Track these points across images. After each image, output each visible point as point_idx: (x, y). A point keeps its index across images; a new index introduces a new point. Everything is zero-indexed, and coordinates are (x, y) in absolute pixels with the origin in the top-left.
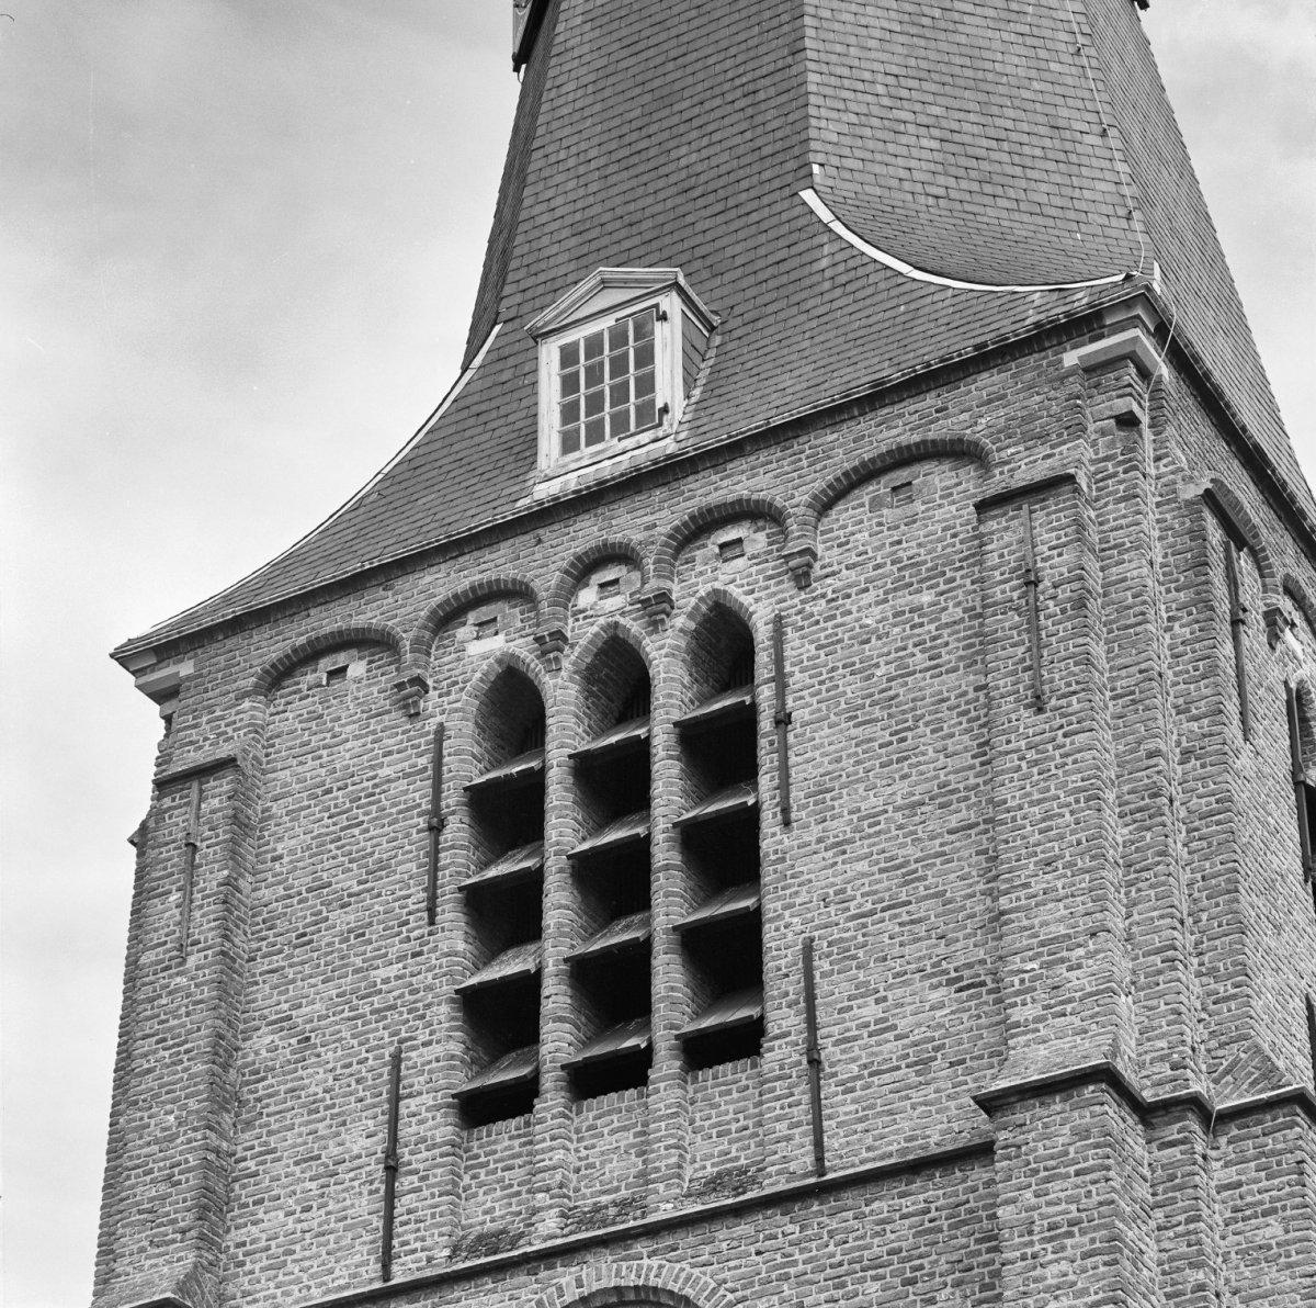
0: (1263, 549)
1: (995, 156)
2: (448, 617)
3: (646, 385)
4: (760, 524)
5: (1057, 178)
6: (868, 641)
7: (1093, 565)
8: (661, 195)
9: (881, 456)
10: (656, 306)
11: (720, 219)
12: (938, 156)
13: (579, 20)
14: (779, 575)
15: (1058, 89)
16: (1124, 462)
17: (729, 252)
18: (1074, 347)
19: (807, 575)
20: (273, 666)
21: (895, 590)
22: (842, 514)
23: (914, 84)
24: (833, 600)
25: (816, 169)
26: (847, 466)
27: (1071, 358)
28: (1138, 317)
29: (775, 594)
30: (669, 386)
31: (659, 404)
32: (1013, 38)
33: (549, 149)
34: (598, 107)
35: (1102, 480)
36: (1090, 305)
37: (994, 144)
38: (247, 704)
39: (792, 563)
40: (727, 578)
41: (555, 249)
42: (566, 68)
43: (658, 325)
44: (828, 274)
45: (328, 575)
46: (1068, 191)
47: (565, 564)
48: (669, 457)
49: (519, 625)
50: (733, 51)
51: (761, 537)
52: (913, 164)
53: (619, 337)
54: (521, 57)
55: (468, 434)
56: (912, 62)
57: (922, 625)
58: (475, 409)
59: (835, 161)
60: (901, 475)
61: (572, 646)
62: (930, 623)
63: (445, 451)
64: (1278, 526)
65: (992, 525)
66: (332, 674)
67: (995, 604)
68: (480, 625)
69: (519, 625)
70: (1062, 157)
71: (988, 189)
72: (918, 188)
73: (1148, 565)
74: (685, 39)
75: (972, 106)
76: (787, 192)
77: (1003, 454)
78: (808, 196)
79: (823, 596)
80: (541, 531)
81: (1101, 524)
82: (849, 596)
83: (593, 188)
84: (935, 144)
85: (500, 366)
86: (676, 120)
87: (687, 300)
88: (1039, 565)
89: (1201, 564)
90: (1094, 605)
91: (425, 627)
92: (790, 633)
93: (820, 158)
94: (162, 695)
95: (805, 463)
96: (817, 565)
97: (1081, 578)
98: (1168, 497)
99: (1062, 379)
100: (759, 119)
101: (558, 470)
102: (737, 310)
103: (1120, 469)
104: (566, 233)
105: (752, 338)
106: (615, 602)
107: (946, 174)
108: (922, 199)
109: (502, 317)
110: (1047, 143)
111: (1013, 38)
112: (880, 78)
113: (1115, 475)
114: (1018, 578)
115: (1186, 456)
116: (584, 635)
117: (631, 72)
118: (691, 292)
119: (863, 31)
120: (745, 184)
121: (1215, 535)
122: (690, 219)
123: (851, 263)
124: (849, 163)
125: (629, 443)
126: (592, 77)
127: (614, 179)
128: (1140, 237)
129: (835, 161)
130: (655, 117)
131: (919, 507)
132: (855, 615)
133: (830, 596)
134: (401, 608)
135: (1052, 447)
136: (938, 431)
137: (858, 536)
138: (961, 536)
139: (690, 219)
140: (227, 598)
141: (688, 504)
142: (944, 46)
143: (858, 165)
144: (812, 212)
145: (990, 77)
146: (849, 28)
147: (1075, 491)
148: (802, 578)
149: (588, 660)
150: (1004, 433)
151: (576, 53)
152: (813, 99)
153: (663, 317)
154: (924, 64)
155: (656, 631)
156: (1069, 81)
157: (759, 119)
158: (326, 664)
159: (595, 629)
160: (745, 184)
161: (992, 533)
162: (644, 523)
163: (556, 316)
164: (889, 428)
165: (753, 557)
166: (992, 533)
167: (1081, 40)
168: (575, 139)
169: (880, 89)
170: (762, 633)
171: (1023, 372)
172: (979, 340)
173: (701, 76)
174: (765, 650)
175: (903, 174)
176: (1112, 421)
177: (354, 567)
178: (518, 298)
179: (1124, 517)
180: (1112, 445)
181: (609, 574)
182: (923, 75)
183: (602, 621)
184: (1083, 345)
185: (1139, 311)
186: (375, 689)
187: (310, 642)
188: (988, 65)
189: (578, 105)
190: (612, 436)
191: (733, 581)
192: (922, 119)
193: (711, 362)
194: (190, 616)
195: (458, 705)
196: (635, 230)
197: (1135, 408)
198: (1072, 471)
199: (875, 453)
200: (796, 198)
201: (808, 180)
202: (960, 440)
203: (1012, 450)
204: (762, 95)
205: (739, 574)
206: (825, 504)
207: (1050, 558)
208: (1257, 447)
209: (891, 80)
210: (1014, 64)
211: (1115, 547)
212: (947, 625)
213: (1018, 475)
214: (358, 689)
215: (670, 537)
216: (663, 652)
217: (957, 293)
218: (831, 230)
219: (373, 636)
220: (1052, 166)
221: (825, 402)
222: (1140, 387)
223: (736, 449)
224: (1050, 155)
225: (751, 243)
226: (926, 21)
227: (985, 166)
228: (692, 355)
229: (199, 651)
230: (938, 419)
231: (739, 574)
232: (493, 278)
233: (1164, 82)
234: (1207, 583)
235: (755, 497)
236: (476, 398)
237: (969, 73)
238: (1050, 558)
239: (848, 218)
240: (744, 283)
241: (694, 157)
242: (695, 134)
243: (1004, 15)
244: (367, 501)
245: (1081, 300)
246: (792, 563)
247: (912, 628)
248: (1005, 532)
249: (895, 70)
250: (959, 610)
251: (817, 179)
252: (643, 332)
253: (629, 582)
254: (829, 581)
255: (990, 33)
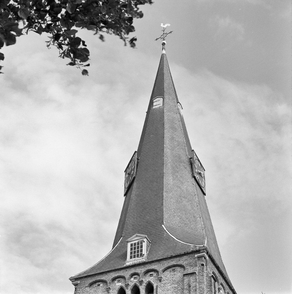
0: (218, 280)
1: (186, 221)
2: (114, 279)
3: (141, 251)
4: (155, 272)
5: (194, 224)
6: (168, 291)
7: (198, 284)
8: (144, 222)
9: (171, 265)
10: (143, 240)
11: (152, 227)
12: (180, 221)
13: (134, 195)
14: (157, 280)
15: (195, 211)
16: (202, 271)
17: (152, 232)
18: (197, 254)
19: (161, 280)
20: (90, 283)
21: (172, 284)
22: (167, 273)
23: (177, 210)
24: (164, 284)
25: (164, 222)
26: (167, 266)
27: (196, 256)
28: (205, 251)
29: (157, 282)
30: (144, 252)
31: (143, 254)
32: (189, 204)
33: (129, 213)
34: (136, 208)
35: (199, 273)
36: (199, 249)
37: (186, 219)
38: (87, 288)
39: (159, 279)
40: (151, 279)
41: (130, 228)
42: (132, 202)
43: (143, 243)
44: (165, 237)
45: (99, 272)
46: (195, 226)
47: (130, 274)
48: (144, 262)
49: (123, 282)
50: (154, 203)
51: (155, 274)
52: (176, 221)
53: (138, 244)
54: (125, 195)
55: (117, 253)
56: (177, 207)
57: (175, 289)
58: (119, 249)
59: (167, 221)
60: (174, 268)
61: (130, 286)
62: (177, 289)
63: (114, 255)
64: (220, 276)
65: (185, 278)
66: (98, 285)
67: (185, 289)
68: (118, 281)
69: (123, 282)
70: (195, 221)
71: (186, 225)
72: (177, 225)
73: (205, 286)
74: (148, 200)
75: (184, 214)
76: (160, 225)
77: (187, 268)
78: (163, 226)
79: (163, 283)
80: (127, 269)
81: (199, 279)
82: (166, 284)
83: (135, 220)
84: (179, 219)
85: (122, 243)
86: (146, 212)
87: (147, 239)
88: (191, 284)
89: (211, 285)
90: (198, 290)
91: (111, 281)
92: (158, 288)
93: (165, 220)
94: (76, 285)
95: (161, 265)
96: (162, 279)
97: (196, 287)
98: (207, 276)
99: (195, 258)
100: (157, 214)
101: (129, 262)
102: (153, 240)
103: (202, 271)
104: (131, 225)
105: (155, 245)
106: (136, 280)
107: (180, 223)
108: (177, 227)
109: (122, 236)
110: (193, 219)
111: (189, 204)
112: (173, 209)
113: (201, 272)
114: (188, 285)
115: (210, 269)
116: (132, 284)
117: (141, 204)
118: (148, 238)
119: (171, 202)
120: (155, 223)
121: (213, 281)
122: (148, 226)
123: (168, 236)
124: (168, 221)
125: (139, 259)
126: (136, 204)
127: (138, 219)
128: (204, 233)
129: (167, 221)
130: (144, 211)
131: (176, 273)
132: (167, 287)
133: (164, 284)
134: (108, 277)
135: (193, 267)
136: (179, 263)
137: (168, 276)
138: (181, 278)
139: (148, 226)
140: (85, 273)
141: (146, 268)
142: (181, 205)
143: (169, 221)
144: (163, 228)
145: (186, 209)
146: (169, 202)
147: (196, 274)
148: (160, 281)
149: (132, 288)
150: (187, 264)
151: (134, 200)
152: (164, 212)
153: (144, 242)
154: (178, 207)
155: (141, 285)
156: (196, 210)
157: (157, 214)
158: (97, 284)
159: (133, 284)
160: (155, 223)
161: (185, 279)
162: (141, 270)
163: (130, 240)
164: (172, 262)
165: (154, 277)
166: (185, 279)
167: (198, 204)
168: (133, 212)
169: (173, 211)
170: (155, 287)
171: (190, 257)
172: (185, 252)
173: (150, 206)
174: (155, 290)
175: (175, 223)
176: (201, 265)
177: (102, 271)
178: (125, 234)
179: (202, 278)
180: (200, 268)
181: (135, 276)
182: (178, 209)
183: (134, 283)
184: (198, 254)
185: (205, 251)
186: (104, 288)
187: (95, 281)
188: (186, 208)
189: (134, 207)
190: (137, 257)
191: (151, 280)
192: (178, 215)
193: (150, 248)
194: (80, 275)
195: (115, 292)
196: (140, 227)
197: (204, 263)
198: (195, 272)
199: (170, 265)
200: (161, 226)
201: (163, 223)
202: (181, 265)
203: (188, 267)
204: (157, 210)
205: (152, 279)
206: (164, 271)
207: (192, 283)
208: (218, 266)
209: (174, 209)
210: (189, 207)
211: (200, 282)
212: (179, 290)
213: (189, 271)
214: (101, 288)
215: (144, 273)
216: (142, 288)
217: (182, 243)
218: (166, 231)
219: (104, 281)
220: (194, 222)
221: (164, 257)
222: (204, 260)
223: (153, 262)
224: (193, 221)
225: (155, 231)
226: (179, 201)
227: (185, 222)
228: (148, 246)
229: (81, 280)
230: (179, 261)
231: (152, 279)
232: (121, 227)
233: (207, 206)
234: (212, 288)
235: (155, 269)
236: (119, 247)
237: (184, 209)
238: (192, 283)
239: (168, 230)
240: (154, 237)
241: (149, 217)
242: (148, 214)
243: (188, 200)
244: (103, 260)
245: (198, 248)
246: (159, 279)
247: (174, 290)
248: (186, 279)
249: (174, 208)
250: (180, 288)
251: (164, 224)
252: (141, 243)
253: (138, 278)
254: (164, 281)
255: (186, 203)
